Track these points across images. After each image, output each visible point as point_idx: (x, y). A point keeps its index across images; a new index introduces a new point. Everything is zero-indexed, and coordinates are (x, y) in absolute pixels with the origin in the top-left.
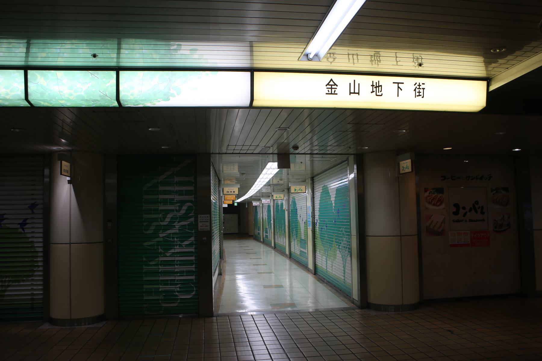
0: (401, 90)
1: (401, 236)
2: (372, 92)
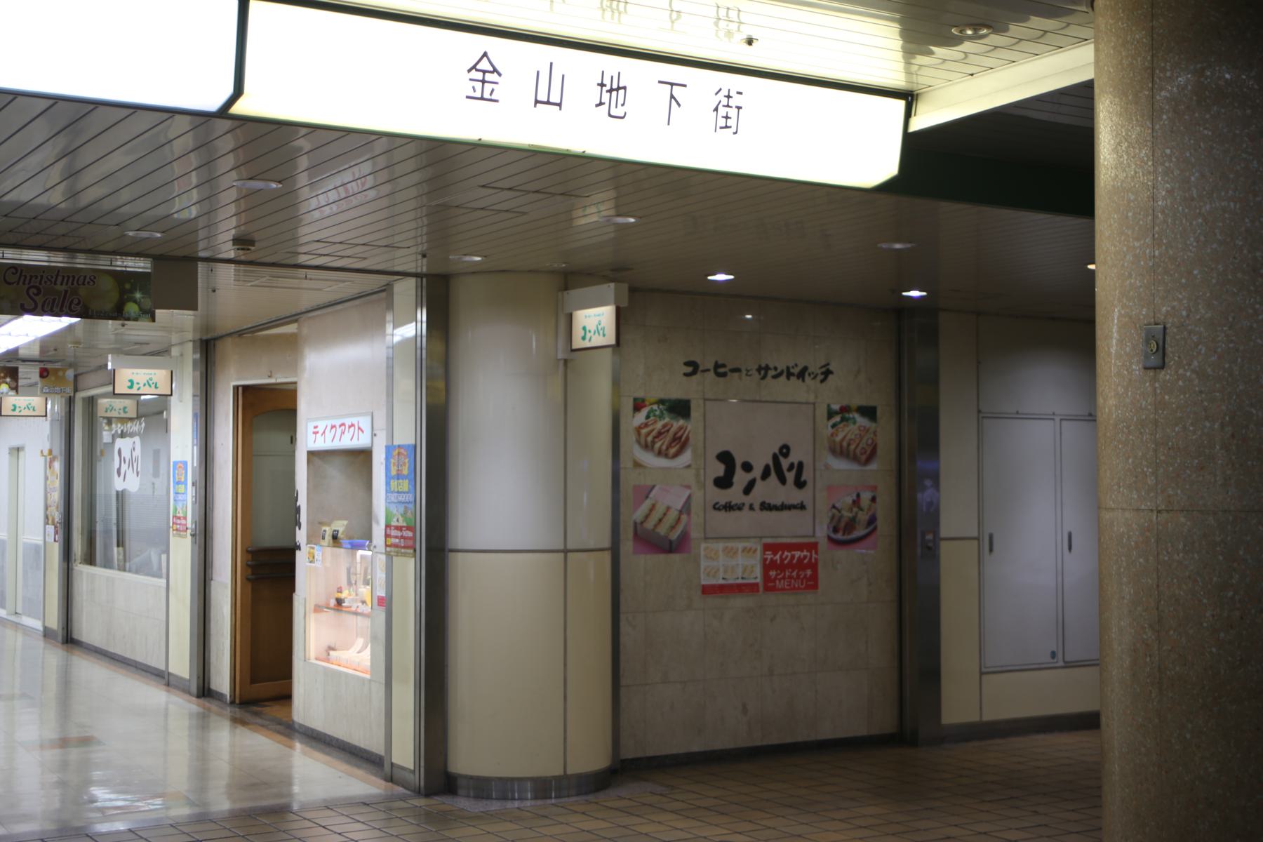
0: (679, 105)
1: (566, 551)
2: (597, 105)
